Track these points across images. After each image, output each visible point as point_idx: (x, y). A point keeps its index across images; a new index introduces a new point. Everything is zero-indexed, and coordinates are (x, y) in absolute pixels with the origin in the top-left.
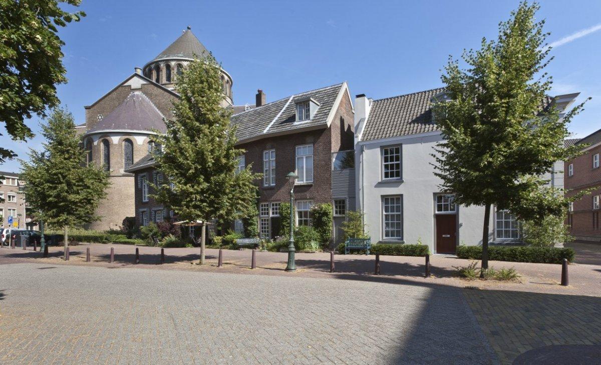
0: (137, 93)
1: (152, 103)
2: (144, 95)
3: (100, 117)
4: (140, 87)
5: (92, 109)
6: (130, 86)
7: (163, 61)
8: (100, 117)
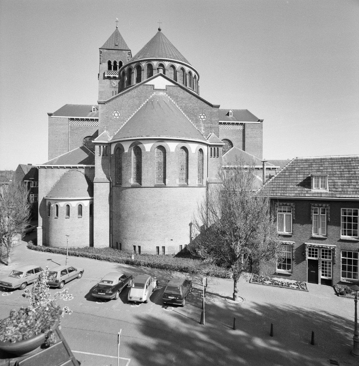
0: (161, 93)
1: (177, 106)
2: (169, 97)
3: (116, 115)
4: (165, 88)
5: (106, 105)
6: (153, 86)
7: (157, 60)
8: (116, 115)
